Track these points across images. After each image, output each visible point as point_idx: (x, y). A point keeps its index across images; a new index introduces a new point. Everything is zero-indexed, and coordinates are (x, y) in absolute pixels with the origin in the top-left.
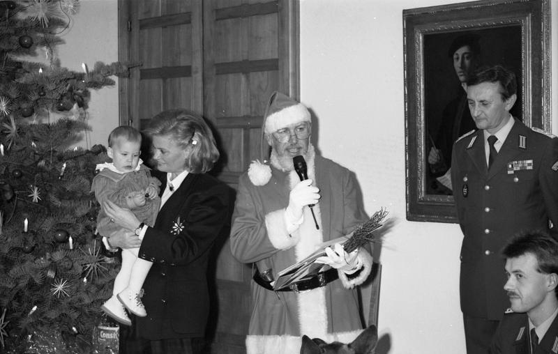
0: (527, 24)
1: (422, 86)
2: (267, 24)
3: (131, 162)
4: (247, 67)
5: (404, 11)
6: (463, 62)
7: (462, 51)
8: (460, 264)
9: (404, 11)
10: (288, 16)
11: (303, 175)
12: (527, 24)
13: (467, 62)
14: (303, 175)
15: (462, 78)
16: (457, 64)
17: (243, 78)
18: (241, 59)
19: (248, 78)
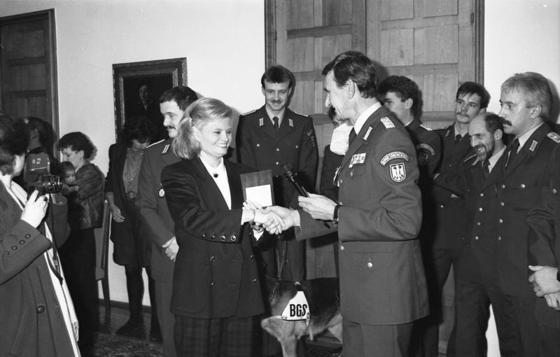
0: (175, 73)
1: (123, 106)
2: (39, 70)
3: (352, 20)
4: (29, 94)
5: (113, 65)
6: (144, 94)
7: (143, 88)
8: (108, 162)
9: (113, 65)
10: (48, 32)
11: (146, 301)
12: (175, 73)
13: (146, 94)
14: (146, 301)
15: (144, 103)
16: (141, 95)
17: (26, 101)
18: (24, 89)
19: (29, 101)
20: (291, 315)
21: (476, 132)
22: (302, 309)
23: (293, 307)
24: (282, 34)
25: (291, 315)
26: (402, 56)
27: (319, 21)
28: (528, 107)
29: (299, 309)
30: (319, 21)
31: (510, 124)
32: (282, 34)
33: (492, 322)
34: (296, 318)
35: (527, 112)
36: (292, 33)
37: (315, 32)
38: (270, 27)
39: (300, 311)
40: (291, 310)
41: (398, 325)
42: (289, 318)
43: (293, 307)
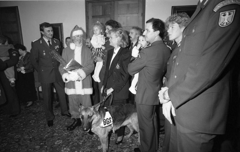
0: (59, 27)
20: (104, 125)
21: (87, 42)
22: (109, 120)
23: (104, 120)
24: (90, 17)
25: (104, 125)
26: (124, 24)
27: (101, 14)
28: (136, 34)
29: (108, 120)
30: (101, 14)
31: (131, 38)
32: (90, 17)
33: (48, 45)
34: (107, 125)
35: (136, 36)
36: (93, 17)
37: (100, 17)
38: (87, 15)
39: (108, 121)
40: (104, 122)
41: (126, 99)
42: (104, 126)
43: (104, 120)
